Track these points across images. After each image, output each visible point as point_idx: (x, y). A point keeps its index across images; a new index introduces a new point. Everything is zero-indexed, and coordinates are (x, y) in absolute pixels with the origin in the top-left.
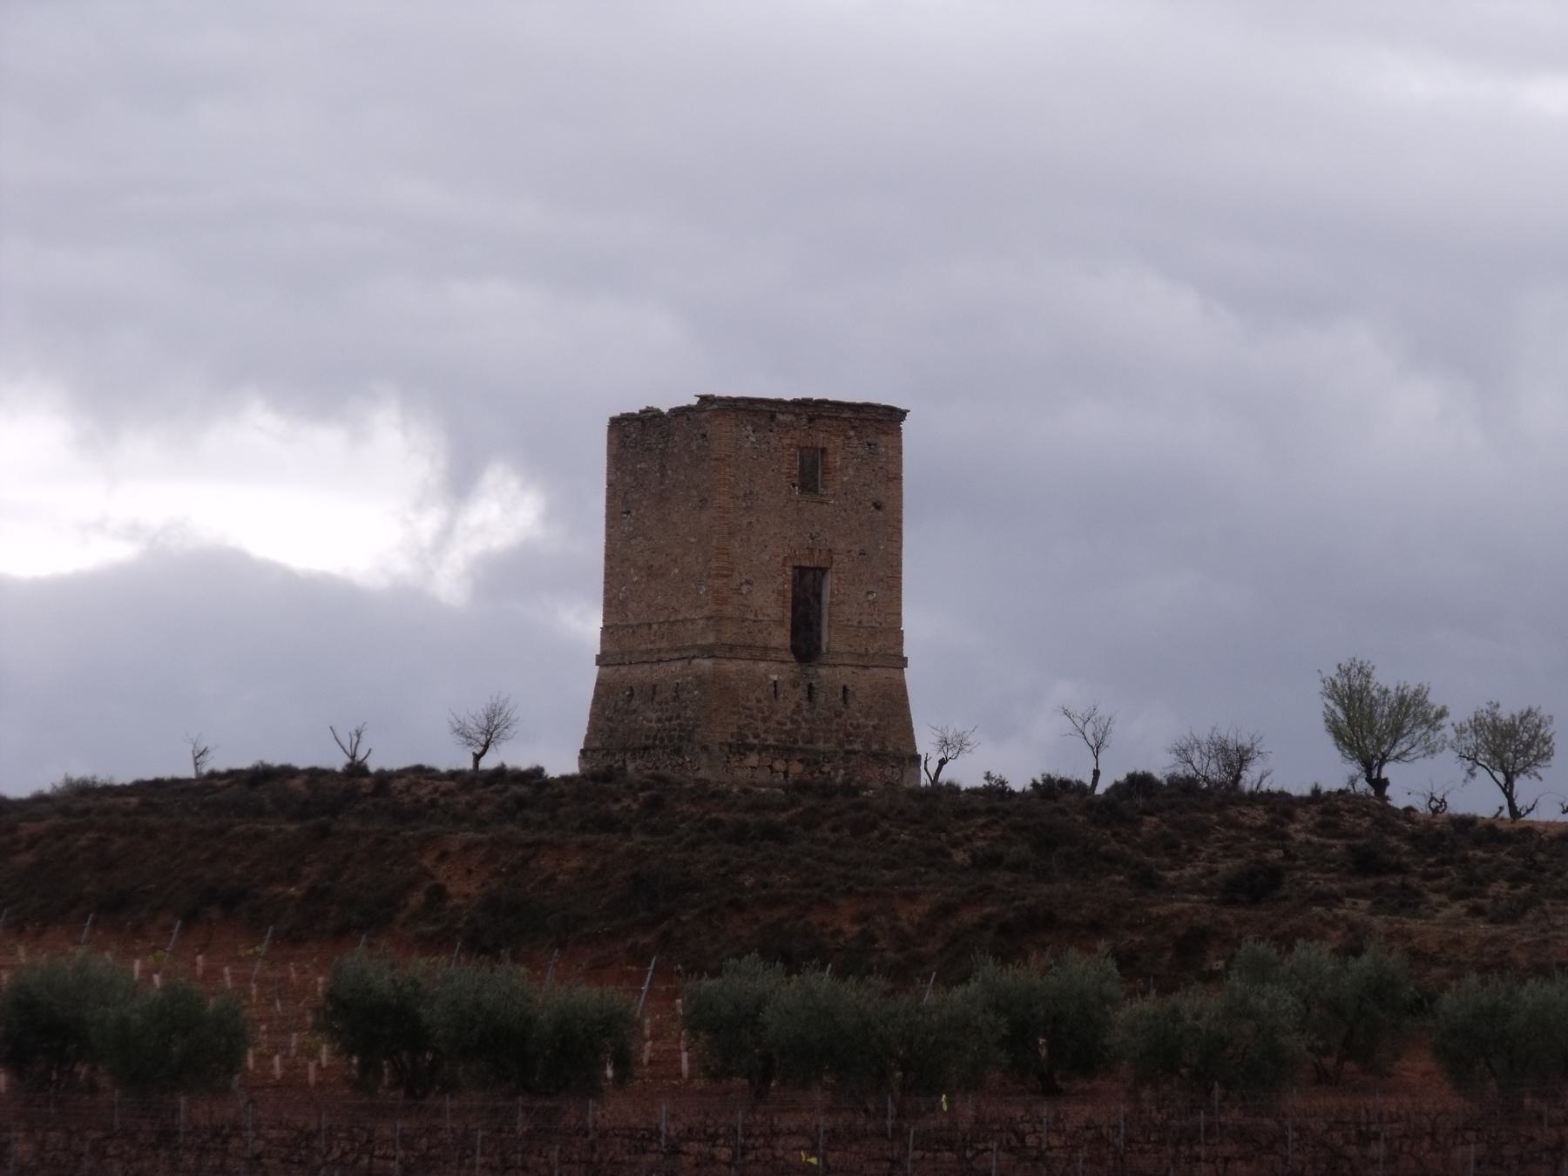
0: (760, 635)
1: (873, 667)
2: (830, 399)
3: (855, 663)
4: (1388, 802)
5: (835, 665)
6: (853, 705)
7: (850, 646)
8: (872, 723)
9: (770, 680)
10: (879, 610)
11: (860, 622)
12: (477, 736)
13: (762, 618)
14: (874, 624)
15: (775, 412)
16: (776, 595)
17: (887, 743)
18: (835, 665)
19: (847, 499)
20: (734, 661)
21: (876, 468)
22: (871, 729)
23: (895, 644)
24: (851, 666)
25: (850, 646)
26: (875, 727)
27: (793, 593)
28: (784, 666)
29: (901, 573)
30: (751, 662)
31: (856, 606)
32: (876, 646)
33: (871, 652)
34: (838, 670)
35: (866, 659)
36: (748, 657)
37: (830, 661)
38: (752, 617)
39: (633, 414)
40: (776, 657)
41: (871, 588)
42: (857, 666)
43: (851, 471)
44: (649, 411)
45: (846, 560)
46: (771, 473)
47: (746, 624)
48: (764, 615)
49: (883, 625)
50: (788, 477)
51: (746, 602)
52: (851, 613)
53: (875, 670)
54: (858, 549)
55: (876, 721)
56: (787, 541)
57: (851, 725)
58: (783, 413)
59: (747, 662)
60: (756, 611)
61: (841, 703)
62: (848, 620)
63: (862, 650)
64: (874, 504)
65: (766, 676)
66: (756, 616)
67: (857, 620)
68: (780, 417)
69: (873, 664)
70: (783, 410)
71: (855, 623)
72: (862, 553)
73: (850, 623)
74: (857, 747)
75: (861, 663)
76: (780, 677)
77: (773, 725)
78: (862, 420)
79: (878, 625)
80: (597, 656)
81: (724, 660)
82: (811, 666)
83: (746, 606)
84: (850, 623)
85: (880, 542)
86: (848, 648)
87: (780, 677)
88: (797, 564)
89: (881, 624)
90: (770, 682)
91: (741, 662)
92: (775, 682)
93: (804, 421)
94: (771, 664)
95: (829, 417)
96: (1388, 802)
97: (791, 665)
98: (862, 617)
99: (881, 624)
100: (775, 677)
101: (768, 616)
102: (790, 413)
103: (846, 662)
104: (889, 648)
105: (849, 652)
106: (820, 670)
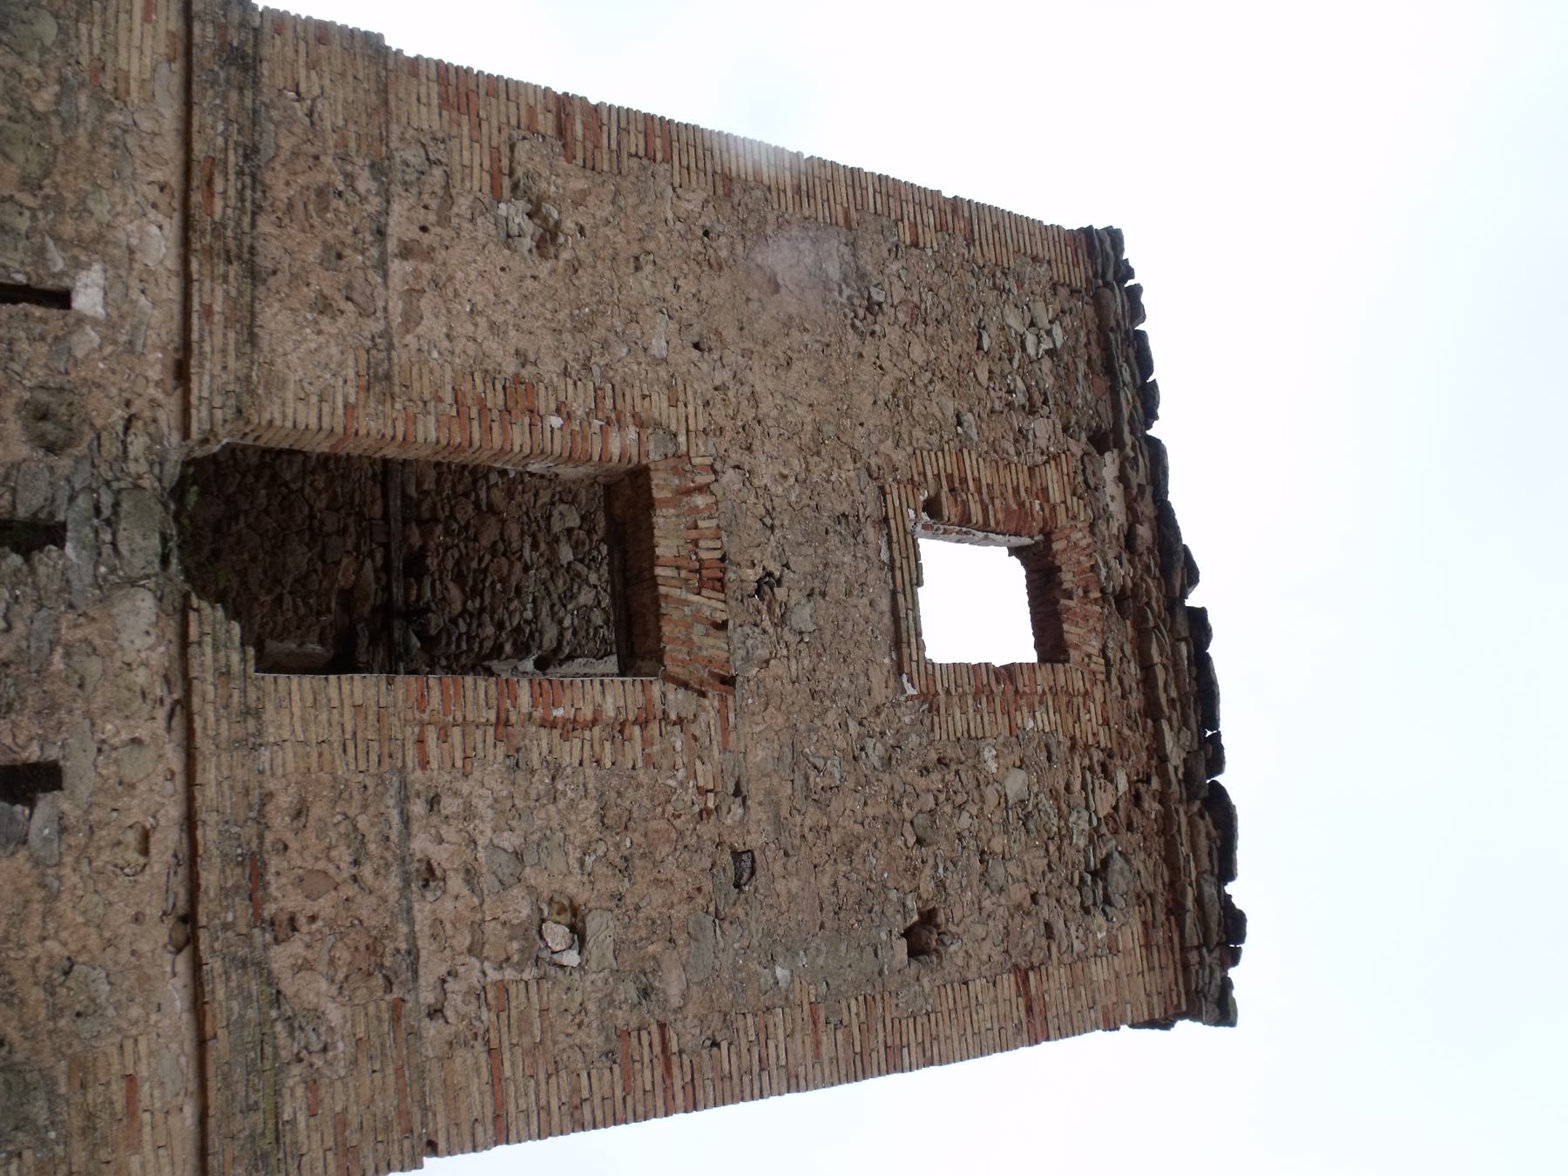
0: (313, 253)
1: (197, 965)
5: (184, 708)
7: (300, 812)
9: (78, 265)
10: (503, 987)
11: (430, 875)
13: (395, 281)
14: (432, 967)
15: (1120, 445)
16: (511, 367)
18: (184, 708)
19: (925, 771)
20: (169, 79)
21: (1046, 910)
23: (341, 1123)
24: (190, 822)
25: (300, 812)
28: (156, 366)
29: (693, 1106)
30: (170, 174)
31: (509, 841)
32: (314, 991)
33: (281, 958)
34: (153, 726)
35: (239, 911)
36: (199, 147)
37: (204, 661)
38: (279, 317)
39: (1122, 250)
40: (208, 312)
41: (600, 927)
42: (191, 858)
43: (1016, 783)
44: (1166, 572)
45: (705, 776)
46: (950, 407)
47: (364, 183)
48: (412, 294)
49: (431, 1029)
50: (950, 477)
51: (463, 205)
52: (469, 813)
53: (176, 995)
54: (754, 840)
56: (735, 456)
58: (1122, 478)
59: (169, 146)
60: (428, 255)
62: (433, 802)
63: (284, 898)
64: (928, 917)
65: (95, 244)
66: (406, 252)
67: (439, 855)
68: (1109, 466)
69: (214, 965)
70: (1132, 474)
71: (421, 844)
72: (744, 866)
73: (418, 808)
75: (210, 879)
76: (92, 336)
78: (1167, 818)
79: (428, 997)
81: (176, 25)
82: (165, 561)
83: (448, 198)
84: (418, 808)
85: (803, 961)
86: (285, 800)
87: (92, 336)
88: (662, 486)
89: (435, 1012)
90: (59, 263)
91: (170, 112)
92: (62, 299)
93: (1122, 573)
94: (171, 290)
95: (1147, 667)
97: (168, 417)
98: (456, 883)
99: (435, 1012)
100: (88, 299)
101: (411, 319)
102: (1130, 508)
103: (209, 773)
104: (312, 1085)
106: (146, 603)
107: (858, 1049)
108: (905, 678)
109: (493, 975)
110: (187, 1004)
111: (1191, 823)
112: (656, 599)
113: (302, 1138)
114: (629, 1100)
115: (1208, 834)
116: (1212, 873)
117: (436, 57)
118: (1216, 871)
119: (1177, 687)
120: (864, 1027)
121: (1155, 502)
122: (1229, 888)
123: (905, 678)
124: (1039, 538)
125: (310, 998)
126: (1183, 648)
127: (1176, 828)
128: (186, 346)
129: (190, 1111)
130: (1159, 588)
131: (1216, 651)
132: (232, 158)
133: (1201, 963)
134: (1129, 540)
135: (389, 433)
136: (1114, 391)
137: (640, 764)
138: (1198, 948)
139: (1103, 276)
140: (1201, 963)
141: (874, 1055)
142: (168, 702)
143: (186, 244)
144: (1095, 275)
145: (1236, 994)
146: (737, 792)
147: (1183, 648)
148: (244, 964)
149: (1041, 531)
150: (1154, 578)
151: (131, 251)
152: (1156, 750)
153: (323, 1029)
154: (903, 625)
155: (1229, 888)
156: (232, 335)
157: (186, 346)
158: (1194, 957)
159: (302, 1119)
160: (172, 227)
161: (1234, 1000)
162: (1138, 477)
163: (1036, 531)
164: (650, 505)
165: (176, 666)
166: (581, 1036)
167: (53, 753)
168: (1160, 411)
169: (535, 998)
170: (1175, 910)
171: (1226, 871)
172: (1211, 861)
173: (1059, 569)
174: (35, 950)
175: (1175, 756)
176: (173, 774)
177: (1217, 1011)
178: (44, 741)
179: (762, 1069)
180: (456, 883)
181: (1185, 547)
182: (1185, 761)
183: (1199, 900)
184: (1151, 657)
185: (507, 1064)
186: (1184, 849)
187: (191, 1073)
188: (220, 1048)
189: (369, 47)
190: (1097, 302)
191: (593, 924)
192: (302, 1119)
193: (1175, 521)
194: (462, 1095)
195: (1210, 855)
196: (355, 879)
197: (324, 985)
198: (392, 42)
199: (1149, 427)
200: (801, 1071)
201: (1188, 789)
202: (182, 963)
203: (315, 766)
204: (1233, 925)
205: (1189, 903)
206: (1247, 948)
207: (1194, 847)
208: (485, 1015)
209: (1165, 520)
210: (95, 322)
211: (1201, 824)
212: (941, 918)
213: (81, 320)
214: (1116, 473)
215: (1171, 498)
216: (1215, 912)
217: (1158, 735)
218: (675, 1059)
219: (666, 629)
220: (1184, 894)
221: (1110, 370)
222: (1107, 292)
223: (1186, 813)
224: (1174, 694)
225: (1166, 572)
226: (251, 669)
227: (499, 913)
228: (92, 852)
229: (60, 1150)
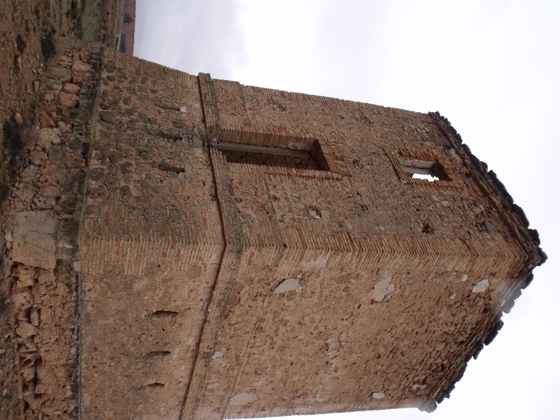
2: (498, 177)
3: (218, 180)
4: (472, 357)
6: (157, 174)
7: (241, 183)
8: (131, 187)
12: (201, 156)
15: (453, 147)
17: (100, 200)
22: (123, 184)
26: (125, 191)
27: (291, 167)
32: (249, 211)
37: (214, 156)
55: (134, 193)
57: (129, 164)
58: (457, 153)
61: (159, 161)
62: (275, 187)
65: (184, 104)
71: (272, 193)
74: (94, 164)
75: (220, 187)
77: (125, 94)
80: (209, 75)
96: (472, 357)
98: (283, 200)
100: (183, 109)
105: (297, 337)
107: (412, 246)
108: (402, 180)
109: (296, 216)
110: (217, 209)
111: (510, 216)
112: (326, 160)
113: (249, 236)
114: (341, 245)
115: (516, 216)
116: (521, 224)
117: (251, 85)
118: (522, 223)
119: (491, 189)
120: (412, 242)
121: (468, 156)
122: (530, 227)
123: (402, 180)
124: (435, 162)
125: (248, 213)
126: (490, 181)
127: (505, 217)
128: (204, 116)
129: (219, 227)
130: (477, 171)
131: (499, 177)
132: (210, 93)
133: (528, 245)
134: (465, 164)
135: (252, 132)
136: (448, 138)
137: (328, 186)
138: (525, 242)
139: (436, 119)
140: (528, 245)
141: (418, 248)
142: (207, 165)
143: (202, 104)
144: (434, 120)
145: (543, 250)
146: (358, 194)
147: (490, 181)
148: (229, 201)
149: (435, 160)
150: (475, 170)
151: (191, 105)
152: (491, 203)
153: (251, 218)
154: (398, 170)
155: (530, 227)
156: (214, 115)
157: (204, 116)
158: (525, 244)
159: (248, 233)
160: (199, 104)
161: (544, 252)
162: (462, 152)
163: (433, 160)
164: (320, 145)
165: (208, 159)
166: (324, 231)
167: (182, 167)
168: (462, 139)
169: (309, 222)
170: (514, 235)
171: (526, 223)
172: (520, 222)
173: (443, 165)
174: (181, 193)
175: (498, 203)
176: (209, 174)
177: (540, 257)
178: (180, 165)
179: (381, 246)
180: (283, 200)
181: (481, 162)
182: (501, 203)
183: (520, 231)
184: (481, 184)
185: (303, 233)
186: (510, 221)
187: (219, 220)
188: (225, 214)
189: (237, 83)
190: (436, 124)
191: (323, 212)
192: (248, 233)
193: (518, 207)
194: (292, 237)
195: (519, 220)
196: (256, 195)
197: (251, 211)
198: (241, 83)
199: (461, 143)
200: (395, 248)
201: (505, 209)
202: (215, 203)
203: (243, 176)
204: (534, 235)
205: (517, 231)
206: (540, 237)
207: (513, 220)
208: (295, 223)
209: (473, 159)
210: (185, 113)
211: (513, 215)
212: (430, 225)
213: (182, 113)
214: (455, 152)
215: (472, 153)
216: (527, 233)
217: (490, 199)
218: (354, 241)
219: (329, 164)
220: (514, 231)
221: (445, 135)
222: (439, 122)
223: (507, 214)
224: (491, 191)
225: (478, 168)
226: (226, 162)
227: (296, 206)
228: (192, 182)
229: (189, 225)
